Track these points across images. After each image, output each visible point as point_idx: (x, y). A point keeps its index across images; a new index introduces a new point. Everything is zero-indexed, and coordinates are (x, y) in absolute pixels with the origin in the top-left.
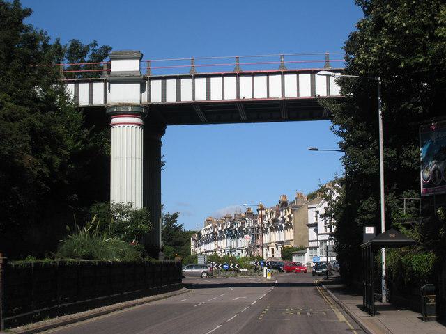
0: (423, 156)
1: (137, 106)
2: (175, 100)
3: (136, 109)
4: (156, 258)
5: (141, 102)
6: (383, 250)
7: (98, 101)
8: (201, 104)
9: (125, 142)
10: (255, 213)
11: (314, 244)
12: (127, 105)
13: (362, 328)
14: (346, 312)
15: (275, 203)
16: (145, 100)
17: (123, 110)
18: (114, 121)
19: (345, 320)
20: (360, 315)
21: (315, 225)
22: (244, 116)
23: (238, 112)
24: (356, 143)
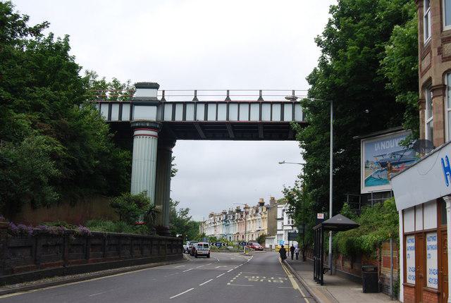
0: (10, 16)
1: (154, 122)
2: (181, 120)
3: (152, 125)
4: (165, 238)
5: (217, 118)
6: (330, 232)
7: (126, 117)
8: (201, 124)
9: (144, 148)
10: (242, 210)
11: (281, 232)
12: (146, 122)
13: (311, 296)
14: (302, 281)
15: (256, 204)
16: (160, 119)
17: (144, 125)
18: (136, 133)
19: (299, 288)
20: (311, 283)
21: (282, 219)
22: (232, 136)
23: (228, 132)
24: (314, 153)
